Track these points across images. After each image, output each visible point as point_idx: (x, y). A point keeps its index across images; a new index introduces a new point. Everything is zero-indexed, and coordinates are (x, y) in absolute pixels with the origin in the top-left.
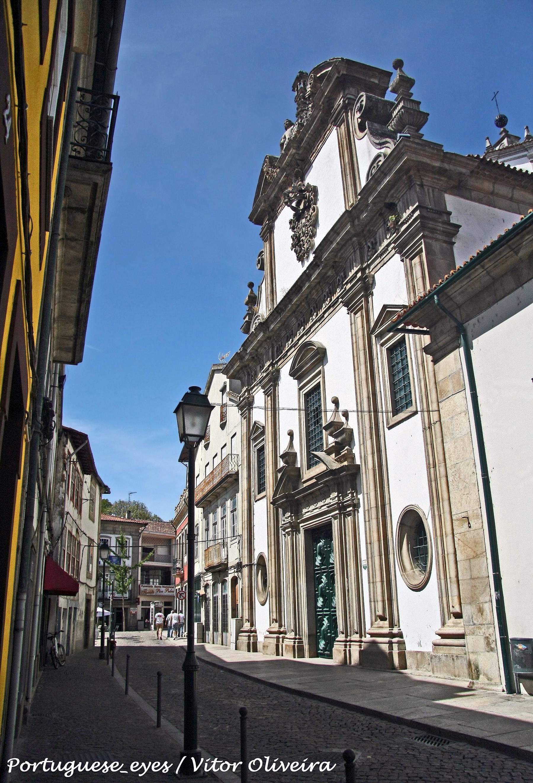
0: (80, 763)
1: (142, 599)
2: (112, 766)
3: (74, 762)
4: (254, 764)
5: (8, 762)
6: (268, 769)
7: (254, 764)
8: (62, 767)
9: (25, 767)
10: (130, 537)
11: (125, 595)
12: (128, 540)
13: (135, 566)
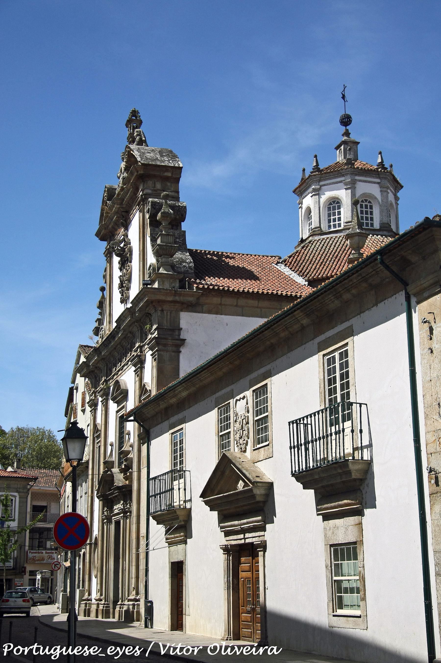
0: (65, 648)
1: (29, 568)
2: (91, 650)
3: (59, 646)
4: (212, 648)
5: (4, 646)
6: (224, 652)
7: (212, 648)
8: (49, 651)
9: (18, 651)
10: (16, 494)
11: (7, 564)
12: (14, 499)
13: (22, 529)
